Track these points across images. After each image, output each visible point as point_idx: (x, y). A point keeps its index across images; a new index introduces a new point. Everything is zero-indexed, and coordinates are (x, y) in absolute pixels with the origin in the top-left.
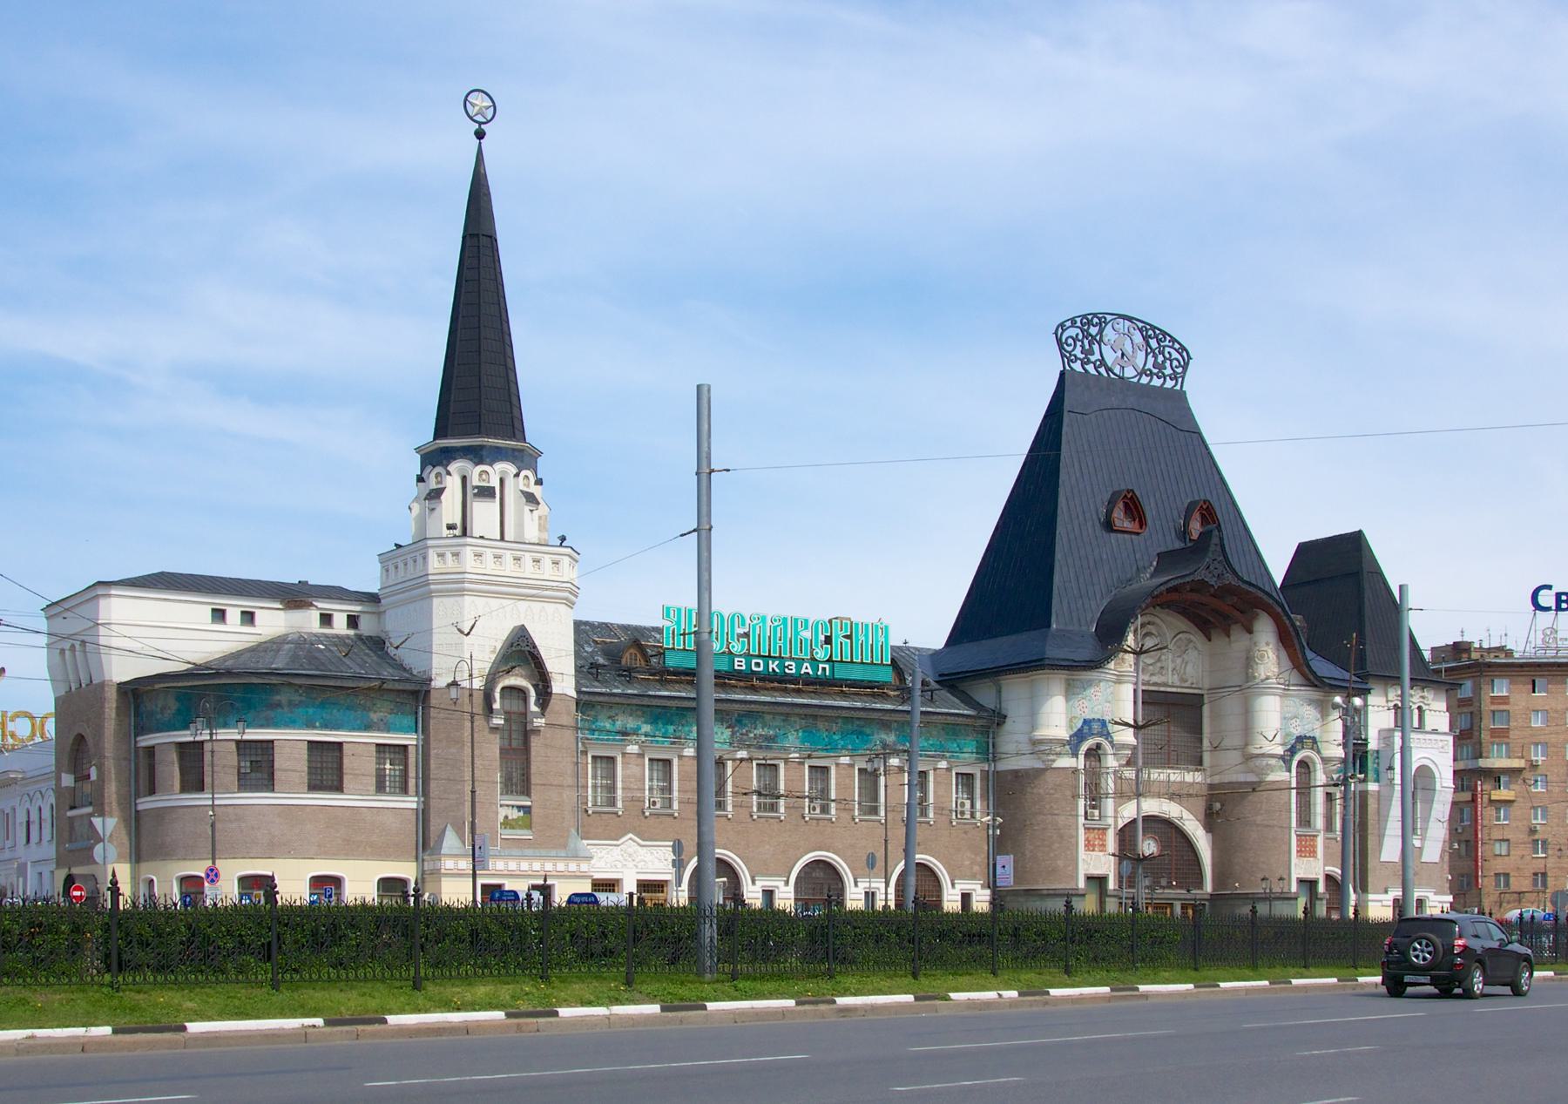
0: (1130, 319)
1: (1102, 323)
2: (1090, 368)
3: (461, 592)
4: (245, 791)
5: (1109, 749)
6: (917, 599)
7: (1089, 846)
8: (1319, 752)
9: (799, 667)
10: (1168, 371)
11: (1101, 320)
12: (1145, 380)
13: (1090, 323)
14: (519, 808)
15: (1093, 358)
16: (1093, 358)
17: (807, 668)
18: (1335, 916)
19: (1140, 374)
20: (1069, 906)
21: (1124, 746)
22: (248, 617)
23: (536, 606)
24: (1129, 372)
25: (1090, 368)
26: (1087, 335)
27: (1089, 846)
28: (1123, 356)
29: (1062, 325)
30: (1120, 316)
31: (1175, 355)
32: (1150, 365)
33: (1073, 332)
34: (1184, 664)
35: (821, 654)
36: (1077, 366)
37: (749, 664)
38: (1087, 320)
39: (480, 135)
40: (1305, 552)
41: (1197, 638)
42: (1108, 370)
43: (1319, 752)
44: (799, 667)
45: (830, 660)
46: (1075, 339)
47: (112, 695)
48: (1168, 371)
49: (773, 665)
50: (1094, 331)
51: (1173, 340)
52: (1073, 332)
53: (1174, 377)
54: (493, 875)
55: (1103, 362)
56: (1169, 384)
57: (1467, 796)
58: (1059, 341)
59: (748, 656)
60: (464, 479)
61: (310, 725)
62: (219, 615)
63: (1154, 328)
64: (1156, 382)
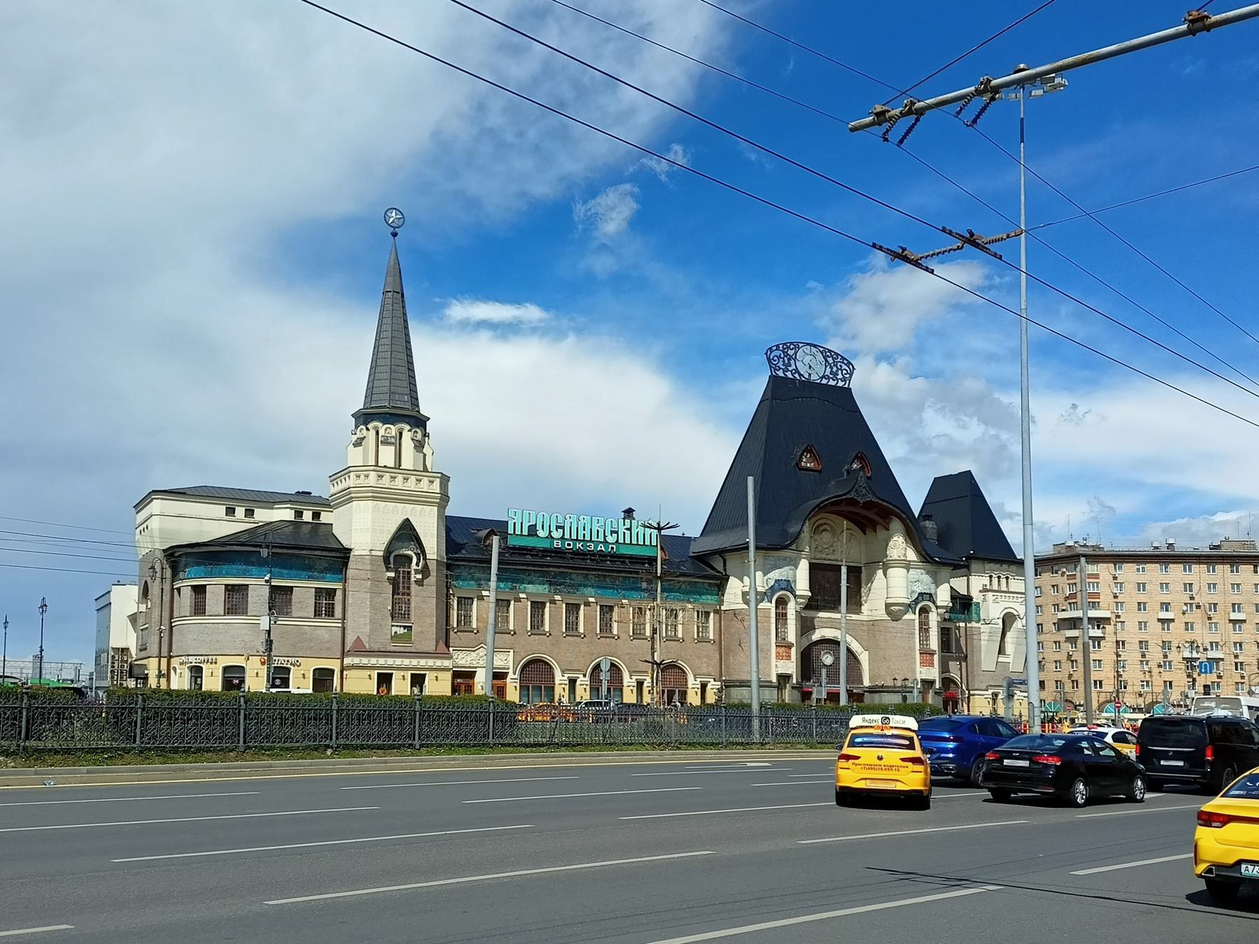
0: (815, 346)
1: (797, 346)
3: (350, 500)
5: (933, 608)
7: (779, 657)
8: (934, 603)
9: (596, 547)
11: (797, 346)
12: (824, 381)
13: (788, 348)
17: (601, 547)
18: (164, 686)
19: (822, 378)
20: (905, 698)
21: (801, 597)
22: (250, 513)
23: (419, 507)
24: (814, 377)
25: (789, 374)
26: (786, 355)
27: (779, 657)
28: (809, 366)
30: (811, 345)
32: (828, 373)
34: (844, 547)
36: (780, 373)
38: (787, 346)
39: (394, 235)
40: (941, 485)
42: (800, 375)
43: (934, 603)
44: (596, 547)
45: (562, 538)
46: (779, 357)
47: (160, 555)
48: (840, 376)
49: (579, 545)
50: (791, 352)
51: (843, 358)
53: (844, 380)
54: (373, 668)
55: (797, 371)
56: (841, 384)
58: (769, 360)
60: (377, 433)
62: (230, 511)
63: (830, 351)
64: (832, 383)
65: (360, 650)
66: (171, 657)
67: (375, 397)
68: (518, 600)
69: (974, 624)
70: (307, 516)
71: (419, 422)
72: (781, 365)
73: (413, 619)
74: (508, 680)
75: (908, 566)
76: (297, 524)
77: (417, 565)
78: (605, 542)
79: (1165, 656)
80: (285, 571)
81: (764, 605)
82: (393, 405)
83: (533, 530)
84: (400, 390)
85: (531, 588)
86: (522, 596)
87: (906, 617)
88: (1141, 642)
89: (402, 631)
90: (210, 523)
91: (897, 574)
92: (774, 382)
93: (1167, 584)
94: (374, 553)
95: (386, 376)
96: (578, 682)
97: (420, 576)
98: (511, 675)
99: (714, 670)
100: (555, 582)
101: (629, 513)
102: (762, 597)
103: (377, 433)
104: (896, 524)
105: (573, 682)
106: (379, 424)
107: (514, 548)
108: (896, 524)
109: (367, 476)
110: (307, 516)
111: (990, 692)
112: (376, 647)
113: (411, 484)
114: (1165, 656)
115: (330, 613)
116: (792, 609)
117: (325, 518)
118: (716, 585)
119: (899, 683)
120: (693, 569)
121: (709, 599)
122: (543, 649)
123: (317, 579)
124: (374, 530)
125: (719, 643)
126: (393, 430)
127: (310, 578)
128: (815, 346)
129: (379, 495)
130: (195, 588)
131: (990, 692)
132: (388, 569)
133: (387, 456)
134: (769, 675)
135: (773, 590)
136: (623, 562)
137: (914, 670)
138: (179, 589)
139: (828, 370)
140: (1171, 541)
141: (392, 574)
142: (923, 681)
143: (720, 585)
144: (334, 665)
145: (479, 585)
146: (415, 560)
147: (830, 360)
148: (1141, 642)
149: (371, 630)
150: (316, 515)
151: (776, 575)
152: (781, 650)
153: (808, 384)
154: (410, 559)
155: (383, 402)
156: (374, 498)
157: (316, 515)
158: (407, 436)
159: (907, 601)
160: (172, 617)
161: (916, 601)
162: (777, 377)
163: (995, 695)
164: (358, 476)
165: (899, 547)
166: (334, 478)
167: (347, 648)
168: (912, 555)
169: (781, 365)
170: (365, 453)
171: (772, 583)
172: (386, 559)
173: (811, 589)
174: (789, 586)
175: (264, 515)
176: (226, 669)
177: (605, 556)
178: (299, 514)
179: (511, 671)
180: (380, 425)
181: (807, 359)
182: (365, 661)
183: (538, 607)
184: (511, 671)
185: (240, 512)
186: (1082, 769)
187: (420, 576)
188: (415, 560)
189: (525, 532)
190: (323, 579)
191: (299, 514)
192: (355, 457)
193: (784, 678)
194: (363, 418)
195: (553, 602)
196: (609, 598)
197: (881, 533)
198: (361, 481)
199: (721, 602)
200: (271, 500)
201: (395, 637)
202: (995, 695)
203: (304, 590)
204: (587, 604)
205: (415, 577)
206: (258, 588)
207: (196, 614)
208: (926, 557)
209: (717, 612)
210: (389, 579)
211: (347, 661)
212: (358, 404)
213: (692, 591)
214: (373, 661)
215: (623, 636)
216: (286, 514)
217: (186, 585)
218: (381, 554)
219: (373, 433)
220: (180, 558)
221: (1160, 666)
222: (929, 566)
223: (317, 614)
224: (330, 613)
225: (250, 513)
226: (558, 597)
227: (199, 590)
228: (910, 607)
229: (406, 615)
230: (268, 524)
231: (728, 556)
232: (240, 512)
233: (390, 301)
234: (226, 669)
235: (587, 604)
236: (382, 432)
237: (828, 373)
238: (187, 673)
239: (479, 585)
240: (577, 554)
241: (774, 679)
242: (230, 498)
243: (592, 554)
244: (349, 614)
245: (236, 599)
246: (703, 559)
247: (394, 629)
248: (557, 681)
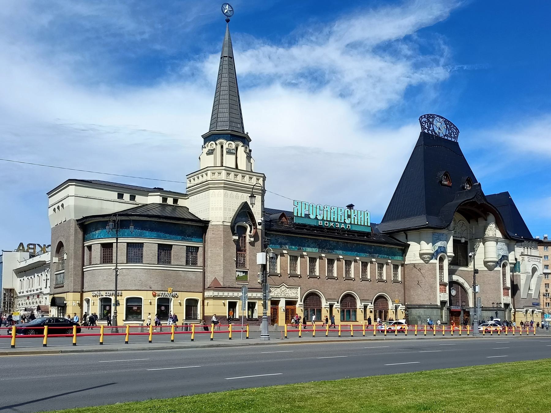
0: (442, 118)
2: (430, 132)
3: (209, 189)
4: (131, 262)
6: (372, 204)
7: (441, 291)
9: (340, 225)
10: (453, 136)
11: (432, 116)
12: (446, 138)
14: (243, 272)
15: (431, 129)
16: (431, 129)
17: (343, 226)
22: (133, 198)
24: (441, 135)
25: (430, 132)
26: (428, 120)
29: (421, 117)
30: (438, 116)
31: (455, 131)
32: (447, 133)
33: (425, 119)
35: (348, 221)
36: (426, 131)
37: (323, 223)
41: (466, 222)
42: (435, 133)
45: (351, 223)
46: (425, 122)
47: (73, 225)
48: (453, 136)
49: (332, 224)
50: (431, 120)
52: (425, 119)
53: (455, 138)
54: (225, 298)
56: (453, 140)
57: (10, 332)
58: (420, 121)
59: (323, 220)
60: (222, 147)
61: (159, 237)
62: (120, 196)
65: (217, 287)
66: (83, 292)
67: (219, 124)
68: (302, 256)
69: (517, 273)
70: (170, 201)
71: (245, 140)
72: (426, 126)
73: (248, 267)
74: (297, 306)
75: (497, 240)
76: (164, 205)
77: (250, 232)
78: (345, 223)
79: (547, 291)
80: (167, 235)
81: (433, 261)
82: (228, 131)
83: (307, 216)
84: (235, 120)
85: (309, 249)
86: (305, 253)
87: (496, 269)
88: (546, 284)
89: (241, 274)
90: (109, 204)
91: (491, 245)
92: (423, 134)
93: (547, 256)
94: (225, 224)
95: (227, 110)
96: (334, 306)
97: (252, 239)
98: (299, 303)
99: (401, 298)
100: (322, 247)
101: (351, 207)
102: (433, 256)
103: (222, 147)
104: (491, 217)
105: (331, 306)
106: (224, 141)
107: (299, 225)
108: (491, 217)
109: (220, 173)
110: (170, 201)
111: (525, 309)
112: (227, 285)
113: (246, 180)
114: (547, 291)
115: (195, 263)
116: (446, 263)
117: (181, 203)
118: (401, 249)
119: (495, 306)
120: (381, 243)
121: (399, 258)
122: (316, 286)
123: (187, 240)
124: (225, 209)
125: (403, 282)
126: (233, 145)
127: (183, 240)
128: (442, 118)
129: (229, 186)
130: (104, 245)
131: (525, 309)
132: (234, 234)
133: (229, 161)
134: (436, 301)
135: (437, 252)
136: (354, 235)
137: (500, 298)
138: (90, 247)
139: (448, 132)
140: (546, 236)
141: (237, 238)
142: (6, 290)
143: (405, 248)
144: (198, 296)
145: (281, 247)
146: (249, 229)
147: (448, 126)
148: (546, 284)
149: (224, 274)
150: (175, 201)
151: (439, 244)
152: (442, 287)
153: (438, 138)
154: (245, 229)
155: (224, 127)
156: (225, 188)
157: (175, 201)
158: (241, 150)
159: (497, 260)
160: (83, 265)
161: (501, 260)
162: (424, 132)
163: (527, 311)
164: (214, 174)
165: (493, 231)
166: (190, 176)
167: (206, 287)
168: (499, 235)
169: (426, 126)
170: (215, 158)
171: (437, 248)
172: (232, 227)
173: (454, 251)
174: (443, 250)
175: (140, 200)
176: (128, 300)
177: (345, 231)
178: (165, 200)
179: (299, 300)
180: (224, 141)
181: (438, 124)
182: (221, 294)
183: (313, 260)
184: (299, 300)
185: (127, 197)
186: (214, 319)
187: (252, 239)
188: (249, 229)
189: (303, 215)
190: (191, 241)
191: (165, 200)
192: (208, 161)
193: (443, 303)
194: (207, 138)
195: (321, 258)
196: (350, 256)
197: (481, 222)
198: (216, 176)
199: (404, 261)
200: (146, 192)
201: (238, 278)
202: (527, 311)
203: (179, 246)
204: (339, 260)
205: (248, 239)
206: (150, 245)
207: (104, 263)
208: (506, 236)
209: (403, 265)
210: (234, 241)
211: (207, 294)
212: (206, 130)
213: (392, 254)
214: (226, 294)
215: (357, 279)
216: (156, 199)
217: (96, 243)
218: (229, 224)
219: (219, 147)
220: (87, 225)
221: (544, 296)
222: (507, 241)
223: (187, 263)
224: (195, 263)
225: (133, 198)
226: (323, 255)
227: (107, 247)
228: (497, 263)
229: (243, 265)
230: (144, 205)
231: (409, 233)
232: (127, 197)
233: (227, 63)
234: (128, 300)
235: (339, 260)
236: (225, 147)
237: (447, 133)
238: (98, 303)
239: (281, 247)
240: (331, 229)
241: (439, 304)
242: (121, 190)
243: (337, 229)
244: (208, 263)
245: (135, 253)
246: (391, 234)
247: (238, 273)
248: (323, 306)
